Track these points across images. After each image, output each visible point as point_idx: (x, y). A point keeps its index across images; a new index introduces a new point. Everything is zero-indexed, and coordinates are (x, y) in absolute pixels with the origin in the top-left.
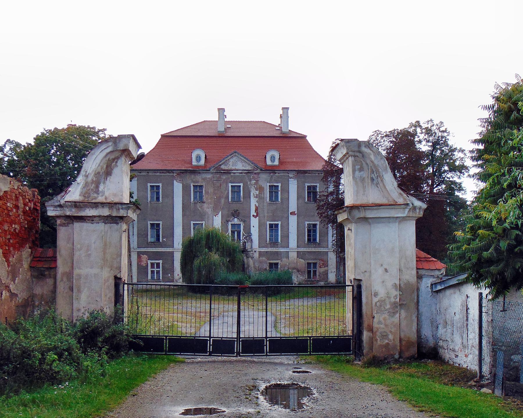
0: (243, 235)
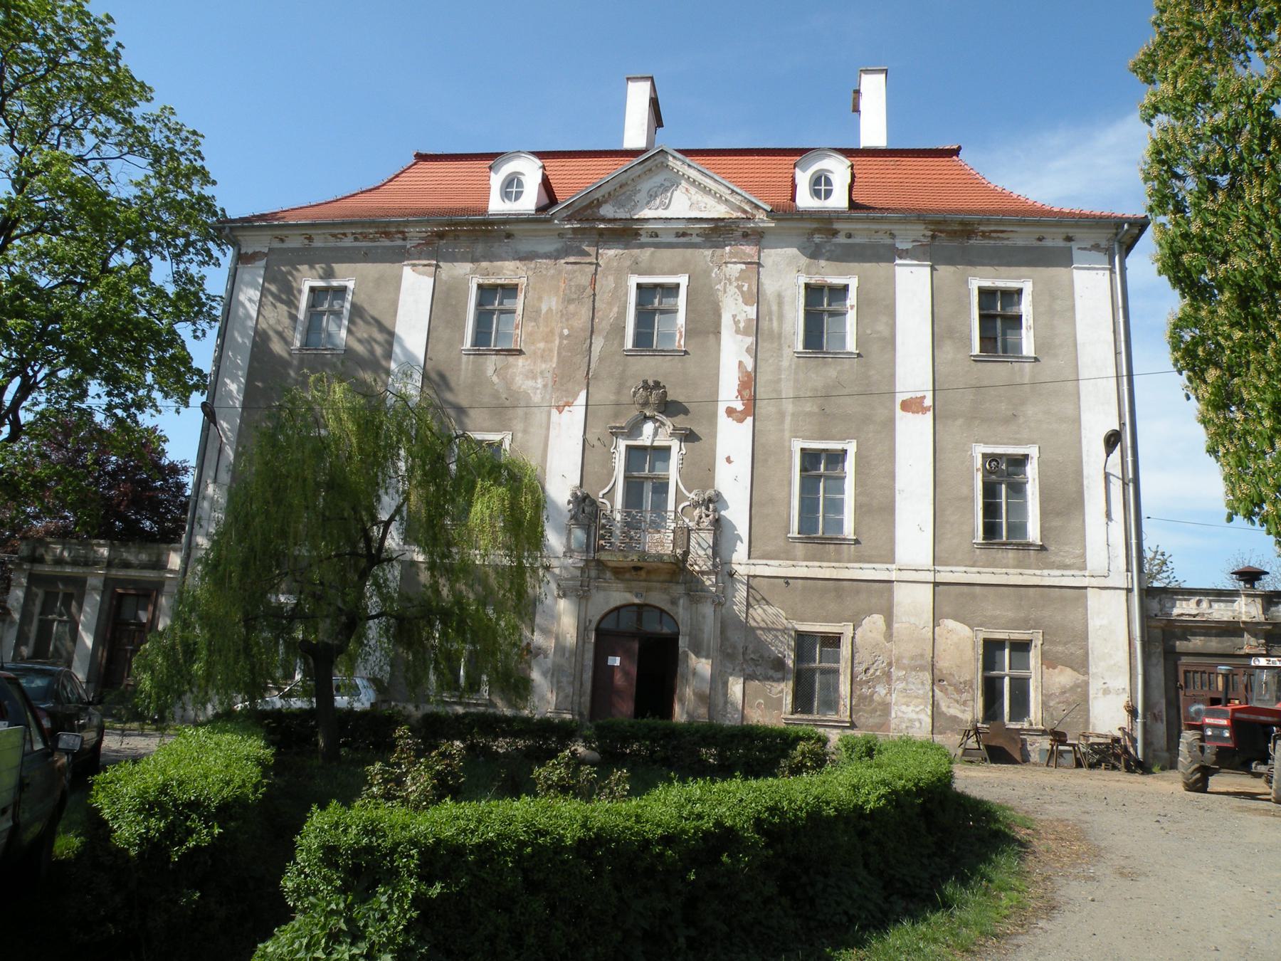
0: (679, 497)
